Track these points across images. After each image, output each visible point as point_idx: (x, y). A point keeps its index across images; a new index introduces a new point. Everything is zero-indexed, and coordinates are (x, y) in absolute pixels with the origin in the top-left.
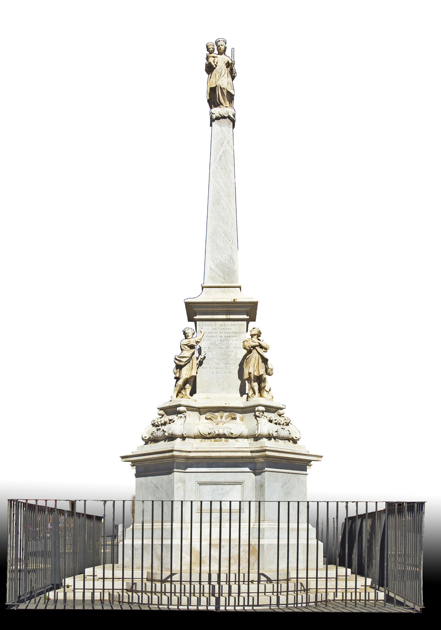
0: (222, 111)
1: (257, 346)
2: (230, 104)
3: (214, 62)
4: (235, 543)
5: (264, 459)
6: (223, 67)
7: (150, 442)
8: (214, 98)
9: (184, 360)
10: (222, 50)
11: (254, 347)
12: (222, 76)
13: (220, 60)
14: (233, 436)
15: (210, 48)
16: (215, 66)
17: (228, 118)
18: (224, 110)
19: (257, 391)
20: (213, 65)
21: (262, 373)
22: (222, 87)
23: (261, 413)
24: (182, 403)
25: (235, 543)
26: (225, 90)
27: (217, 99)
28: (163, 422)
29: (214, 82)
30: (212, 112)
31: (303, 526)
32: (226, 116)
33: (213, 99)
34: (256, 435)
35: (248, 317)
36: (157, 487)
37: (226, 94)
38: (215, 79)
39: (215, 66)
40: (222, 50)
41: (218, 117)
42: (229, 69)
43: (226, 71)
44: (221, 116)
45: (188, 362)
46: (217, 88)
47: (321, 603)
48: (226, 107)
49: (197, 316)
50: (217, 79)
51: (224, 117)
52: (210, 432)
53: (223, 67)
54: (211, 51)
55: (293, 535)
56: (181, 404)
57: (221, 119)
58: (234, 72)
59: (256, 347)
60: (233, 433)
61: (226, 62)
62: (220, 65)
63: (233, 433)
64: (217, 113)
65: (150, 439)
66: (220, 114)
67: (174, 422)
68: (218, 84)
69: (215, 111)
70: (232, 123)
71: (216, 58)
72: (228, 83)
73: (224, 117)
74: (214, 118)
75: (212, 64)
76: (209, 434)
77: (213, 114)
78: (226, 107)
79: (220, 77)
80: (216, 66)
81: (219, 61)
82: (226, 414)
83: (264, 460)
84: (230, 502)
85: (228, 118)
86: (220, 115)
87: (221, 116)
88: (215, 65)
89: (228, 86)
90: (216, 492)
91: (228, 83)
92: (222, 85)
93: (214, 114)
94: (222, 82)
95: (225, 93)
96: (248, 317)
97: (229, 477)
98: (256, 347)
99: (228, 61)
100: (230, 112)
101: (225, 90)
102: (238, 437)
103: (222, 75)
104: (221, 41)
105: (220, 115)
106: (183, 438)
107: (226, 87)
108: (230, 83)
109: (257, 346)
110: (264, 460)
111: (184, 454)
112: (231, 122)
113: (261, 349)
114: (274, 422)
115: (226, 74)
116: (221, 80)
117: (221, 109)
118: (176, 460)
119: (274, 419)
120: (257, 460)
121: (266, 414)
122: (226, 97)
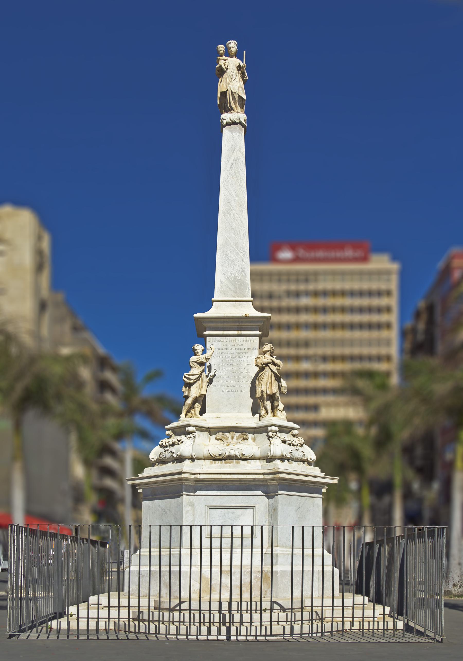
0: (233, 116)
1: (270, 363)
2: (241, 109)
3: (225, 65)
4: (247, 570)
5: (277, 482)
6: (234, 70)
7: (157, 464)
8: (224, 103)
9: (194, 377)
10: (233, 52)
11: (267, 364)
12: (233, 80)
13: (231, 63)
14: (245, 458)
15: (221, 51)
16: (225, 69)
17: (239, 124)
18: (235, 115)
19: (270, 411)
20: (224, 68)
21: (276, 391)
22: (233, 91)
23: (275, 433)
24: (191, 423)
25: (247, 570)
26: (236, 94)
27: (228, 104)
28: (171, 443)
29: (225, 86)
30: (223, 118)
31: (318, 551)
32: (238, 121)
33: (224, 104)
34: (268, 456)
35: (261, 333)
36: (165, 511)
37: (237, 99)
38: (225, 83)
39: (225, 69)
40: (233, 52)
41: (229, 122)
42: (240, 72)
43: (238, 75)
44: (232, 122)
45: (197, 380)
46: (228, 92)
47: (247, 76)
48: (237, 112)
49: (207, 331)
50: (228, 83)
51: (235, 123)
52: (220, 454)
53: (234, 70)
54: (221, 54)
55: (308, 561)
56: (190, 424)
57: (232, 125)
58: (246, 76)
59: (269, 365)
60: (244, 455)
61: (237, 66)
62: (231, 68)
63: (244, 455)
64: (227, 119)
65: (157, 461)
66: (231, 119)
67: (182, 442)
68: (229, 88)
69: (226, 116)
70: (244, 129)
71: (227, 61)
72: (239, 87)
73: (235, 123)
74: (224, 124)
75: (222, 67)
76: (220, 455)
77: (224, 119)
78: (237, 112)
79: (231, 81)
80: (227, 69)
81: (230, 64)
82: (237, 434)
83: (277, 483)
84: (242, 526)
85: (239, 124)
86: (231, 121)
87: (232, 122)
88: (226, 68)
89: (239, 90)
90: (227, 516)
91: (239, 87)
92: (233, 89)
93: (225, 119)
94: (233, 86)
95: (236, 98)
96: (261, 333)
97: (241, 501)
98: (269, 365)
99: (240, 64)
100: (242, 117)
101: (236, 94)
102: (250, 459)
103: (233, 79)
104: (232, 43)
105: (231, 121)
106: (192, 459)
107: (238, 91)
108: (242, 87)
109: (270, 363)
110: (277, 483)
111: (193, 476)
112: (242, 128)
113: (274, 366)
114: (288, 442)
115: (237, 78)
116: (232, 84)
117: (232, 114)
118: (185, 482)
119: (288, 439)
120: (269, 483)
121: (279, 434)
122: (237, 102)
